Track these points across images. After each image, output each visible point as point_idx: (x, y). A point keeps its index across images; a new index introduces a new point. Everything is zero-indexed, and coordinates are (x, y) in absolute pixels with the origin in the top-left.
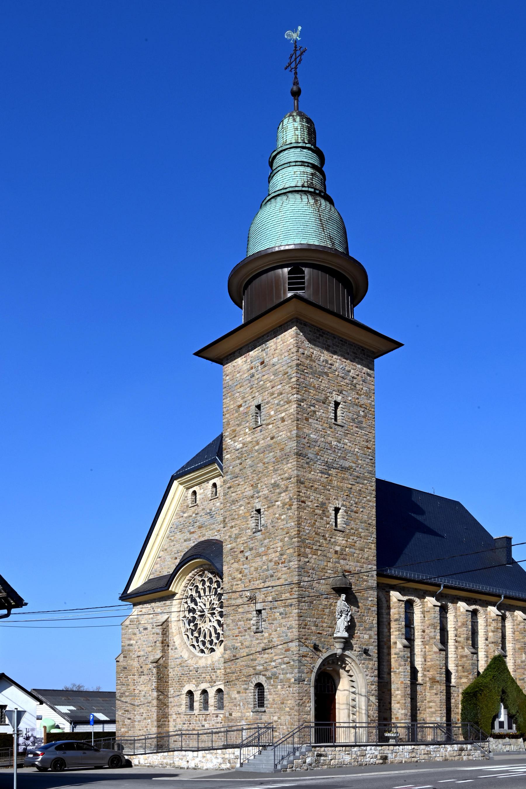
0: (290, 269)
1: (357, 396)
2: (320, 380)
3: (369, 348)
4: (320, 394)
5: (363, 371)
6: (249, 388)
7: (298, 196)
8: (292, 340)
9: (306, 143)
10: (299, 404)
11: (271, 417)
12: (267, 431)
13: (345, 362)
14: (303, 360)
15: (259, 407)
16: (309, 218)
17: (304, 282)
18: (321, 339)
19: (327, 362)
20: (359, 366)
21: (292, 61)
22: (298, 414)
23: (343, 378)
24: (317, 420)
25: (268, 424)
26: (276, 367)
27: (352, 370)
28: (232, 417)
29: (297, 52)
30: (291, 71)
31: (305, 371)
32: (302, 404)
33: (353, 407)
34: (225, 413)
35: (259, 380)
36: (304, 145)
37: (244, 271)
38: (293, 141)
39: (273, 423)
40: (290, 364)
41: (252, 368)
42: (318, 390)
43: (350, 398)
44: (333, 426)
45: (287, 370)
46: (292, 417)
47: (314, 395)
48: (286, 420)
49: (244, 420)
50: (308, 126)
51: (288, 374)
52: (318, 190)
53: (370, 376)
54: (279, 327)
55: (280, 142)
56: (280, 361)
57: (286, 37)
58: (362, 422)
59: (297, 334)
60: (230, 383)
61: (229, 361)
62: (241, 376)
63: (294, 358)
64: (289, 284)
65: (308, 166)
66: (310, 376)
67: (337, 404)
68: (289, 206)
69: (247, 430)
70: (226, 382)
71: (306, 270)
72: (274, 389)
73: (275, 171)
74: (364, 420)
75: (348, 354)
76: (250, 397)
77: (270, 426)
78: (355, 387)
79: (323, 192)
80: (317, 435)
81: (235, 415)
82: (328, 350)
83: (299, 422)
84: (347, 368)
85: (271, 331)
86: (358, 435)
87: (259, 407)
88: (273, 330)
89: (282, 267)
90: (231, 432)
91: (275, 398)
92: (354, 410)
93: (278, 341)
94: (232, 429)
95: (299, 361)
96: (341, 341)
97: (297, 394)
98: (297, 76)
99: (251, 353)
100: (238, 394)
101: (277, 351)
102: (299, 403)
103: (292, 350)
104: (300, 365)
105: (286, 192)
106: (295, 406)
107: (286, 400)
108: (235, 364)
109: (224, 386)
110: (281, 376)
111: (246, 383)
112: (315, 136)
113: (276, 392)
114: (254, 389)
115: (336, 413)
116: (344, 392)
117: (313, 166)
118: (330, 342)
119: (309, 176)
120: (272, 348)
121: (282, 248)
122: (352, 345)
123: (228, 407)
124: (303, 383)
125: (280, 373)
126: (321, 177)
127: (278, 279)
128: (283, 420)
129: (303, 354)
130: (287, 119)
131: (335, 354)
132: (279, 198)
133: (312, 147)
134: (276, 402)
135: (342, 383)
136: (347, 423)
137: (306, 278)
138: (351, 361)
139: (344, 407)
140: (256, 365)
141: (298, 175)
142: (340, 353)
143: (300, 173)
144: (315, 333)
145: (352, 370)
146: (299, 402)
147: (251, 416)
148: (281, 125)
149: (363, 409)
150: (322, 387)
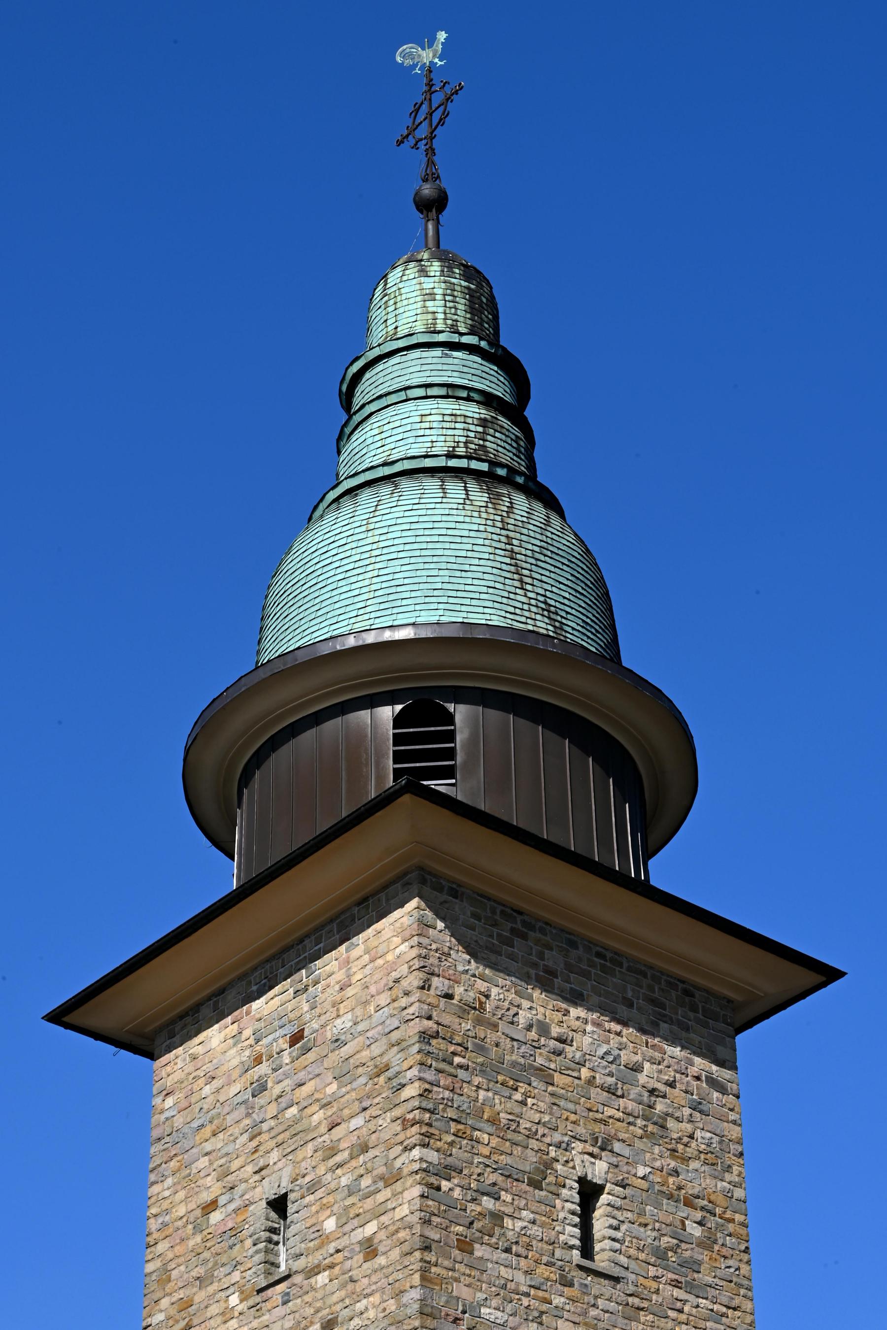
0: (399, 708)
1: (673, 1164)
2: (518, 1096)
3: (716, 989)
4: (517, 1151)
5: (693, 1071)
6: (246, 1136)
7: (432, 484)
8: (404, 947)
9: (461, 334)
10: (430, 1186)
11: (324, 1239)
12: (307, 1298)
13: (619, 1034)
14: (446, 1019)
15: (279, 1205)
16: (469, 547)
17: (453, 750)
18: (519, 947)
19: (544, 1029)
20: (677, 1051)
21: (418, 121)
22: (426, 1222)
23: (611, 1091)
24: (507, 1250)
25: (315, 1271)
26: (345, 1051)
27: (647, 1065)
28: (178, 1250)
29: (435, 98)
30: (415, 146)
31: (457, 1060)
32: (445, 1185)
33: (658, 1206)
34: (155, 1235)
35: (284, 1101)
36: (455, 338)
37: (237, 723)
38: (420, 327)
39: (331, 1267)
40: (395, 1036)
41: (258, 1060)
42: (510, 1135)
43: (641, 1171)
44: (578, 1277)
45: (385, 1059)
46: (402, 1235)
47: (495, 1150)
48: (381, 1249)
49: (224, 1259)
50: (468, 288)
51: (389, 1074)
52: (502, 465)
53: (722, 1089)
54: (359, 904)
55: (378, 334)
56: (361, 1027)
57: (399, 59)
58: (699, 1263)
59: (424, 924)
60: (179, 1121)
61: (177, 1039)
62: (218, 1091)
63: (411, 1010)
64: (398, 757)
65: (468, 399)
66: (477, 1080)
67: (590, 1193)
68: (398, 512)
69: (234, 1300)
70: (163, 1117)
71: (461, 712)
72: (338, 1132)
73: (357, 418)
74: (703, 1256)
75: (631, 1005)
76: (250, 1169)
77: (322, 1279)
78: (663, 1127)
79: (521, 474)
80: (509, 1308)
81: (191, 1243)
82: (546, 987)
83: (431, 1257)
84: (625, 1057)
85: (331, 921)
86: (683, 1317)
87: (279, 1205)
88: (337, 916)
89: (373, 702)
90: (173, 1311)
91: (340, 1166)
92: (662, 1216)
93: (355, 953)
94: (176, 1296)
95: (430, 1023)
96: (599, 955)
97: (425, 1146)
98: (436, 159)
99: (256, 1005)
100: (204, 1162)
101: (350, 992)
102: (433, 1180)
103: (404, 983)
104: (436, 1035)
105: (393, 477)
106: (417, 1191)
107: (382, 1170)
108: (200, 1050)
109: (155, 1134)
110: (363, 1080)
111: (236, 1115)
112: (496, 318)
113: (343, 1145)
114: (264, 1137)
115: (586, 1226)
116: (617, 1147)
117: (488, 400)
118: (554, 959)
119: (472, 428)
120: (332, 980)
121: (370, 638)
122: (645, 976)
123: (167, 1212)
124: (448, 1104)
125: (360, 1070)
126: (516, 431)
127: (357, 747)
128: (370, 1249)
129: (449, 996)
130: (399, 269)
131: (575, 1004)
132: (365, 495)
133: (483, 344)
134: (344, 1181)
135: (609, 1112)
136: (633, 1265)
137: (459, 738)
138: (643, 1031)
139: (619, 1202)
140: (275, 1048)
141: (435, 425)
142: (595, 999)
143: (440, 418)
144: (495, 924)
145: (647, 1065)
146: (432, 1178)
147: (249, 1242)
148: (381, 287)
149: (698, 1215)
150: (524, 1124)
